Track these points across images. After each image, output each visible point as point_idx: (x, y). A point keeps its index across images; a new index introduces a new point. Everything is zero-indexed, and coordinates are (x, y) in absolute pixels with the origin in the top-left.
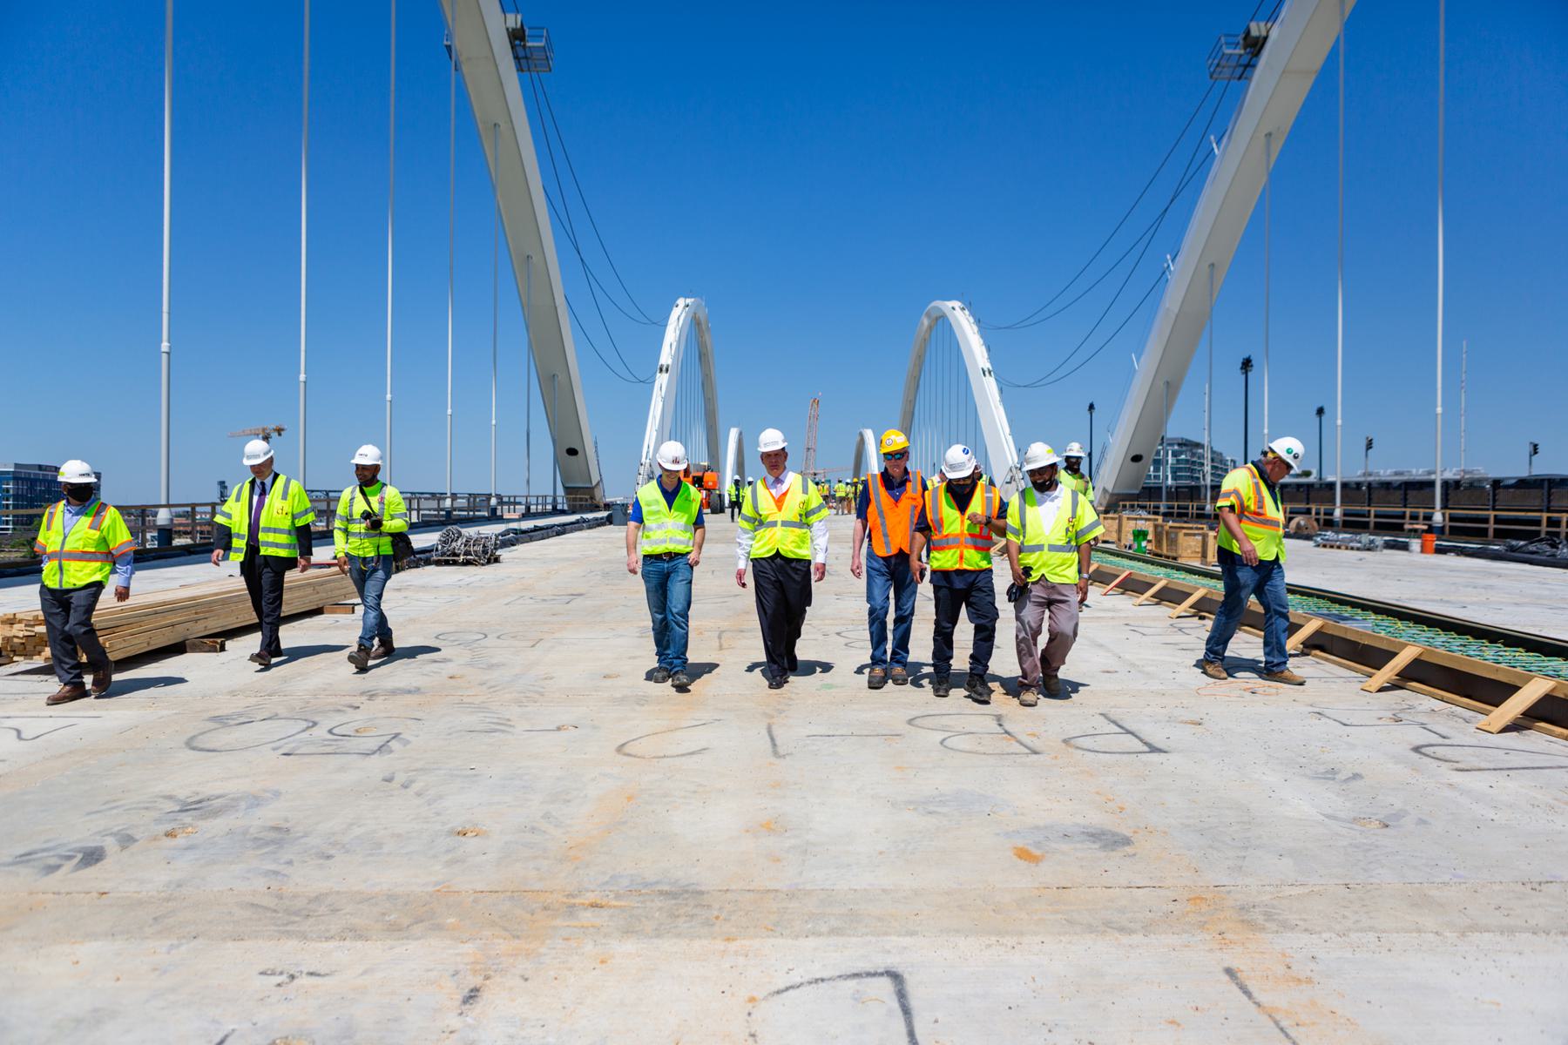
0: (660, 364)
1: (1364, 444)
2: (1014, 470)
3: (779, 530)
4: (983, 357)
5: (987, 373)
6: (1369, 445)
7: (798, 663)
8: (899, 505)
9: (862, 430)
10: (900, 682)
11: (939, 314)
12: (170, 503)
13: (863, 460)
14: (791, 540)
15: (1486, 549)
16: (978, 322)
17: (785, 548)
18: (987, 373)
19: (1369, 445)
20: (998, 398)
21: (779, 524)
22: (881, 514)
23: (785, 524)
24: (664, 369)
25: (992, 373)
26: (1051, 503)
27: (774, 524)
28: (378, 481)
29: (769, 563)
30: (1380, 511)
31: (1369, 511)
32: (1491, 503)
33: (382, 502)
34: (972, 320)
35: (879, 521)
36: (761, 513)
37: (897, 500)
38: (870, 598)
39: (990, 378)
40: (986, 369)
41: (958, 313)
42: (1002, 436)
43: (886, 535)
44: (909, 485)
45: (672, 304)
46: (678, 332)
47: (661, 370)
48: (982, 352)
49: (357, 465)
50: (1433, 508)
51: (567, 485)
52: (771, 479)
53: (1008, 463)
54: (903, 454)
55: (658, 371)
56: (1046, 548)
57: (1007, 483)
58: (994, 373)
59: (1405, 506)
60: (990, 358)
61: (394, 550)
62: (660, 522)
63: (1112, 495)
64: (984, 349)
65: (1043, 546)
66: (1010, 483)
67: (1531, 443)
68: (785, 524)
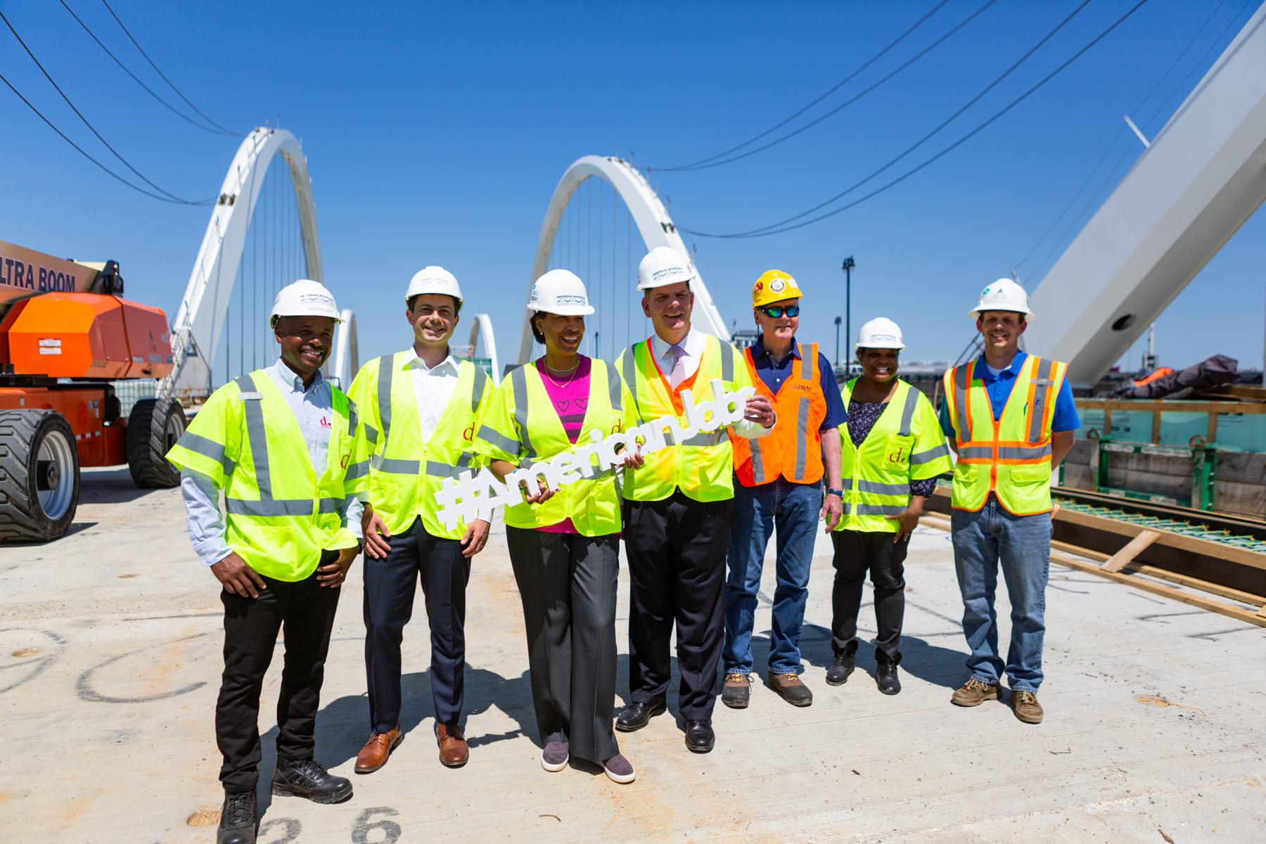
4: (659, 210)
5: (668, 228)
7: (619, 660)
9: (477, 315)
12: (280, 492)
15: (1160, 404)
16: (646, 171)
18: (668, 228)
24: (228, 201)
39: (673, 235)
44: (797, 365)
45: (254, 126)
46: (253, 157)
47: (223, 202)
52: (662, 347)
54: (788, 307)
55: (219, 199)
56: (423, 468)
60: (670, 213)
64: (658, 201)
65: (417, 463)
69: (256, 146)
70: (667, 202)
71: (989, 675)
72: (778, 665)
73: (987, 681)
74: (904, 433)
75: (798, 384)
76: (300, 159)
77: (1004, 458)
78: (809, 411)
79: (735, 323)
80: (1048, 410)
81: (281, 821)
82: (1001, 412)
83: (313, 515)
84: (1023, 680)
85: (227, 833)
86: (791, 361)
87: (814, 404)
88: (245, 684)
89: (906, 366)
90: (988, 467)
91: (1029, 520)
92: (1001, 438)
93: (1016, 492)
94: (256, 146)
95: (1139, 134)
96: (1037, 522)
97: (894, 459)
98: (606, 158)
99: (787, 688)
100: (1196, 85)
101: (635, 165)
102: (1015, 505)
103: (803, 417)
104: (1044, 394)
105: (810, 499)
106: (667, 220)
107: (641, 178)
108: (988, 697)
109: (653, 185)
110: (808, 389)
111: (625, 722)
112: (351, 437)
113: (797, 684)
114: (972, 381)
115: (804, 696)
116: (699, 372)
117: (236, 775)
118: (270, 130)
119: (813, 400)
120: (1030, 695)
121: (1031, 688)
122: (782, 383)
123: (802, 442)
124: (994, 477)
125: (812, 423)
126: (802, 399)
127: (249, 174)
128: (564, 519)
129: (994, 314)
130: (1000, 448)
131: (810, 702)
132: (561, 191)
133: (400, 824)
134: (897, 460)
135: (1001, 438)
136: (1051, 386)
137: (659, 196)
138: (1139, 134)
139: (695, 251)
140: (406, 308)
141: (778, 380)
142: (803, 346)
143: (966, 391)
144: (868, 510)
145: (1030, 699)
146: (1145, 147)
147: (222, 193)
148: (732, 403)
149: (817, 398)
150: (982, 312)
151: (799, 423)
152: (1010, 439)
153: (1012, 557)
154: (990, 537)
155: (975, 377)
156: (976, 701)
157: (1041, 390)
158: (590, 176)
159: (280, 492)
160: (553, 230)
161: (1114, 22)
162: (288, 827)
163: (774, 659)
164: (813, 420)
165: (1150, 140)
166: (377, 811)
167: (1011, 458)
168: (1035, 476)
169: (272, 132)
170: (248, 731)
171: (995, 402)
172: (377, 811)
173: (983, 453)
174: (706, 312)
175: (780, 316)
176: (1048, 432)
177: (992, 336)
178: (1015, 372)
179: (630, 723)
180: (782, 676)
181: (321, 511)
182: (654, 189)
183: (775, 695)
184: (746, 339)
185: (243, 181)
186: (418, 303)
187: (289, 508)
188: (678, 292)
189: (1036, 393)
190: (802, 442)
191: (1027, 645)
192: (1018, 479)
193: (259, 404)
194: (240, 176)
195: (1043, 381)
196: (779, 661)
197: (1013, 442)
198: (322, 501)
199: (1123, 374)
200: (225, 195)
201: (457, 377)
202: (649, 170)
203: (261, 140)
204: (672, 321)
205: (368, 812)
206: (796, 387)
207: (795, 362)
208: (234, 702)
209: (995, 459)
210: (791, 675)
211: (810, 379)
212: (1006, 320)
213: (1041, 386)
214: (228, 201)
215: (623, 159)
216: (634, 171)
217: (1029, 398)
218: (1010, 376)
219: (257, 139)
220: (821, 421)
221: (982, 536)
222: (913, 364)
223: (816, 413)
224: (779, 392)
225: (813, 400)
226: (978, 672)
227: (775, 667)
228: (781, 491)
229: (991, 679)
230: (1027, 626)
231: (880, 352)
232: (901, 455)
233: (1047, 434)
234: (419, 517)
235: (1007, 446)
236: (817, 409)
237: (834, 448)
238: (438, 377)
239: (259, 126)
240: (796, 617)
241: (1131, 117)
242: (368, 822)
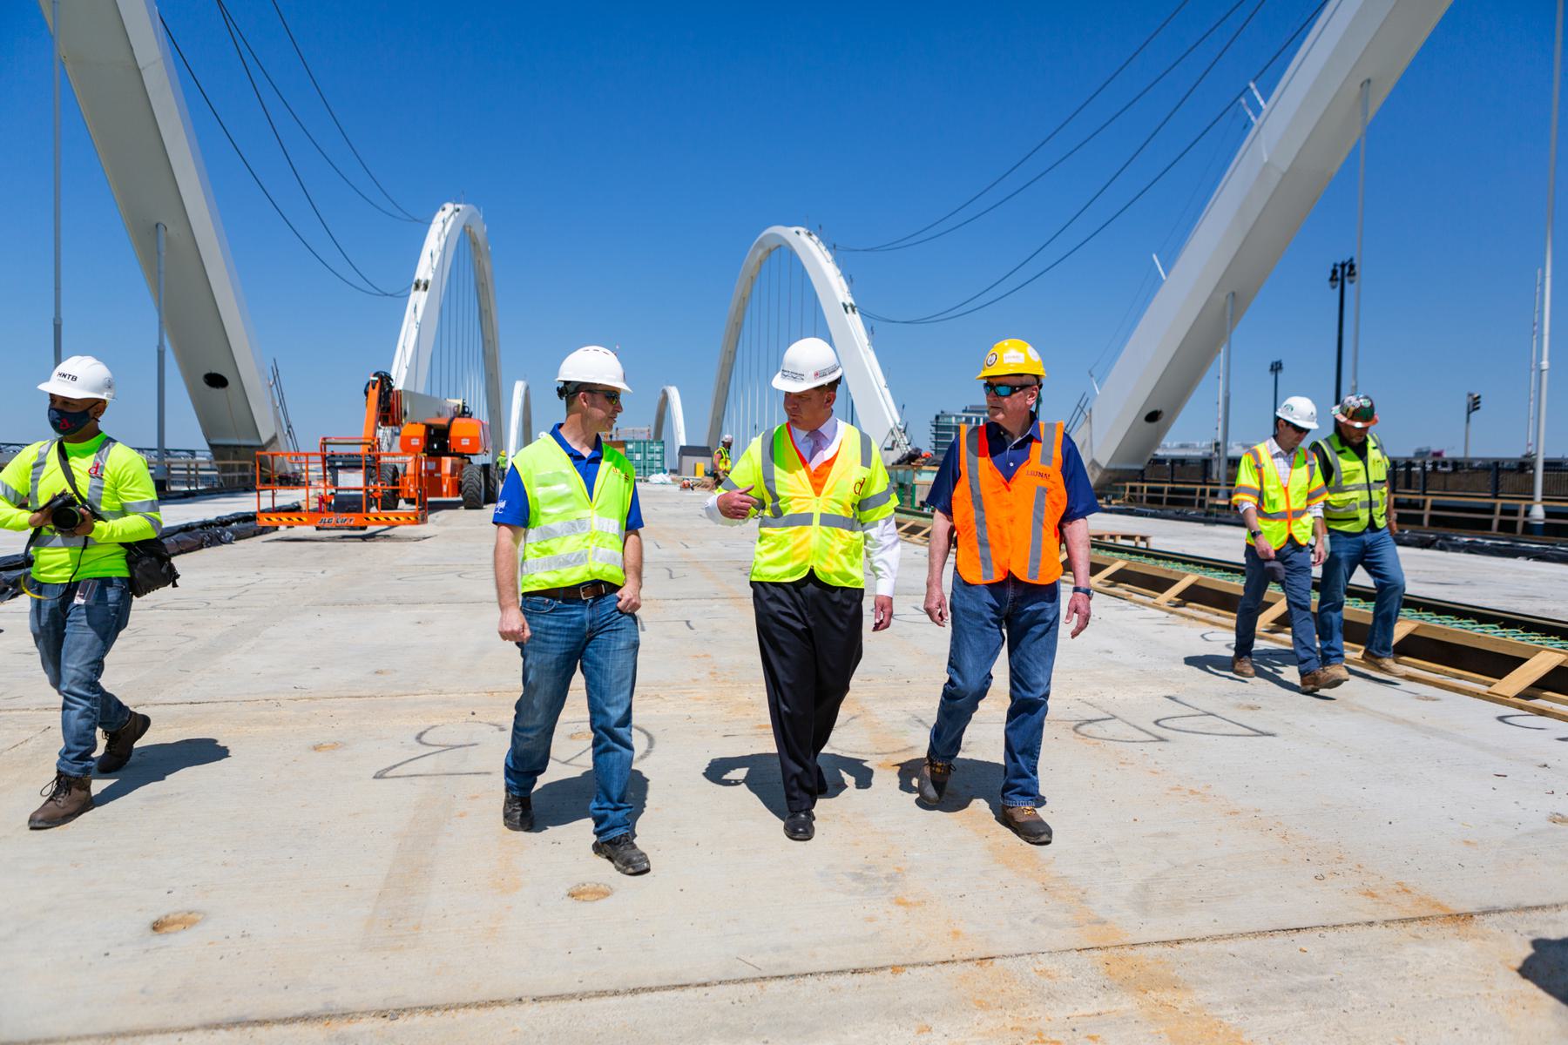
0: (416, 278)
1: (1464, 403)
2: (896, 432)
3: (815, 531)
4: (843, 290)
5: (849, 309)
6: (1475, 404)
8: (1013, 485)
9: (665, 387)
11: (775, 243)
13: (666, 420)
14: (839, 550)
16: (832, 248)
17: (826, 568)
18: (849, 309)
19: (1475, 404)
21: (816, 520)
22: (978, 502)
23: (827, 520)
24: (422, 287)
25: (856, 309)
27: (805, 519)
28: (99, 432)
29: (791, 596)
30: (1438, 501)
31: (1424, 501)
32: (1421, 487)
33: (96, 472)
34: (823, 248)
35: (973, 515)
36: (779, 492)
37: (1009, 475)
38: (954, 664)
39: (855, 316)
40: (847, 304)
41: (804, 237)
42: (878, 391)
43: (984, 544)
44: (1036, 448)
45: (437, 206)
46: (443, 240)
48: (840, 283)
49: (53, 397)
50: (1532, 499)
51: (215, 441)
53: (889, 425)
55: (414, 286)
57: (886, 449)
58: (859, 308)
59: (1496, 497)
60: (852, 292)
61: (1006, 762)
62: (572, 517)
63: (1106, 471)
64: (842, 279)
66: (892, 449)
68: (827, 520)
70: (849, 281)
72: (1011, 796)
75: (1035, 470)
76: (480, 230)
78: (1047, 502)
79: (904, 407)
86: (1029, 444)
89: (1175, 448)
95: (1160, 269)
99: (1023, 823)
101: (823, 239)
103: (1039, 507)
106: (849, 300)
107: (827, 254)
109: (839, 262)
110: (1047, 476)
113: (1034, 819)
115: (1041, 831)
119: (1051, 490)
122: (1017, 468)
127: (440, 258)
131: (1049, 839)
137: (844, 274)
138: (1160, 269)
139: (873, 333)
141: (1012, 464)
142: (1047, 425)
147: (427, 293)
148: (705, 472)
151: (1035, 514)
158: (779, 246)
160: (744, 298)
161: (1075, 215)
163: (1007, 788)
174: (880, 396)
180: (1017, 809)
182: (839, 266)
183: (1008, 831)
184: (978, 415)
185: (435, 266)
190: (1037, 537)
194: (432, 261)
196: (1012, 791)
199: (1447, 458)
200: (418, 280)
206: (1032, 474)
210: (1028, 808)
211: (1050, 464)
214: (422, 287)
215: (812, 232)
220: (1060, 514)
222: (1182, 447)
224: (1012, 479)
227: (1008, 798)
228: (1015, 588)
236: (1056, 500)
240: (1033, 735)
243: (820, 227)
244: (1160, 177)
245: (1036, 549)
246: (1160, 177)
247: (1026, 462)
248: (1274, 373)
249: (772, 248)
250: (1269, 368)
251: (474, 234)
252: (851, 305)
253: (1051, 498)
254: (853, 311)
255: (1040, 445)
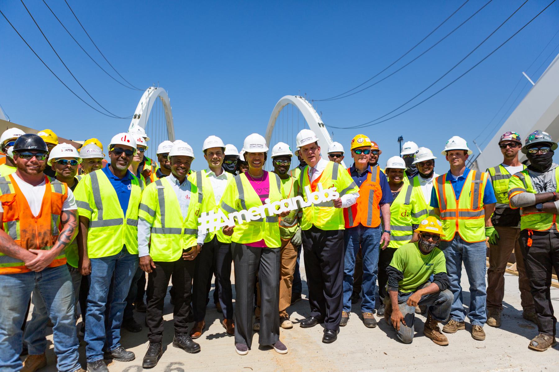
0: (135, 114)
4: (317, 118)
5: (321, 125)
10: (371, 326)
12: (167, 226)
16: (312, 101)
18: (321, 125)
20: (330, 139)
26: (429, 185)
34: (307, 102)
44: (369, 175)
46: (148, 99)
47: (135, 117)
48: (316, 116)
55: (134, 116)
60: (322, 119)
64: (317, 114)
67: (223, 201)
69: (149, 94)
71: (459, 318)
73: (459, 321)
74: (407, 203)
76: (167, 100)
77: (462, 216)
78: (374, 195)
80: (481, 194)
81: (135, 366)
82: (459, 196)
83: (181, 235)
84: (476, 320)
85: (147, 358)
87: (376, 193)
88: (156, 299)
90: (454, 221)
91: (476, 244)
92: (460, 207)
93: (468, 232)
94: (149, 94)
95: (529, 79)
96: (480, 245)
97: (403, 215)
98: (294, 96)
100: (554, 58)
101: (306, 99)
102: (468, 238)
103: (371, 198)
104: (479, 188)
105: (374, 234)
106: (321, 122)
107: (309, 104)
108: (459, 328)
109: (314, 107)
110: (374, 186)
111: (304, 323)
112: (199, 203)
114: (445, 182)
116: (530, 193)
117: (153, 336)
118: (155, 88)
119: (376, 191)
120: (479, 327)
121: (480, 324)
123: (370, 209)
124: (457, 225)
125: (376, 201)
126: (371, 190)
127: (146, 105)
128: (261, 239)
129: (452, 152)
130: (459, 212)
132: (275, 111)
133: (185, 369)
134: (405, 216)
135: (460, 207)
136: (482, 183)
137: (317, 111)
138: (529, 79)
140: (204, 154)
141: (360, 182)
143: (443, 185)
144: (394, 238)
145: (480, 329)
146: (533, 85)
149: (378, 190)
150: (447, 151)
151: (369, 201)
152: (464, 208)
153: (469, 262)
154: (457, 253)
155: (447, 180)
156: (454, 331)
157: (477, 185)
158: (288, 104)
159: (167, 226)
162: (138, 369)
164: (376, 200)
165: (535, 83)
166: (176, 363)
167: (465, 216)
168: (477, 225)
169: (156, 89)
170: (158, 319)
171: (456, 191)
172: (176, 363)
173: (452, 214)
175: (361, 154)
176: (481, 204)
177: (452, 161)
178: (465, 178)
179: (305, 324)
181: (185, 233)
185: (144, 109)
186: (208, 152)
187: (171, 231)
188: (311, 147)
189: (475, 187)
190: (370, 209)
191: (478, 302)
192: (468, 226)
193: (163, 191)
194: (142, 107)
195: (478, 181)
197: (465, 209)
198: (185, 229)
201: (227, 179)
202: (313, 101)
203: (151, 92)
204: (310, 159)
205: (172, 364)
207: (369, 174)
208: (152, 307)
209: (457, 217)
211: (375, 181)
212: (457, 154)
213: (477, 183)
215: (302, 97)
216: (306, 101)
217: (471, 189)
218: (462, 179)
219: (150, 92)
220: (379, 200)
221: (454, 252)
223: (378, 197)
225: (376, 191)
226: (454, 316)
229: (460, 319)
230: (478, 293)
231: (397, 170)
232: (406, 213)
233: (481, 205)
234: (215, 235)
235: (463, 211)
236: (378, 195)
237: (387, 212)
238: (220, 180)
239: (151, 86)
241: (525, 73)
242: (171, 368)
243: (306, 94)
244: (406, 65)
245: (370, 214)
246: (406, 65)
247: (365, 181)
248: (399, 142)
249: (284, 105)
250: (397, 140)
251: (165, 102)
252: (322, 124)
253: (376, 194)
254: (323, 126)
255: (371, 174)
